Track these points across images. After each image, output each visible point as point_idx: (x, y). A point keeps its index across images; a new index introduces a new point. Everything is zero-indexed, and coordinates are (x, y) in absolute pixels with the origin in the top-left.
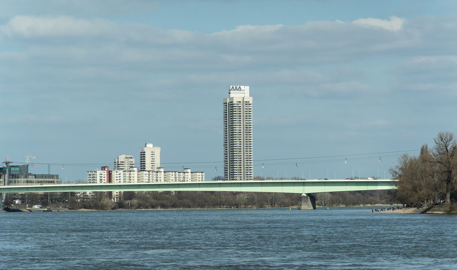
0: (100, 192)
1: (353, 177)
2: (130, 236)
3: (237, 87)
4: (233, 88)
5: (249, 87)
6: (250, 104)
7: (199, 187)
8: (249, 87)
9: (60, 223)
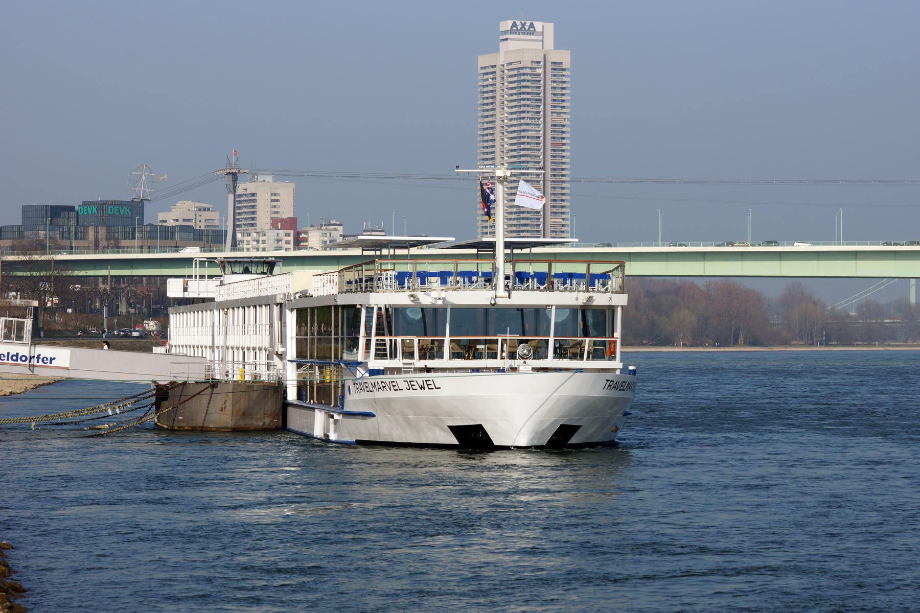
0: (702, 345)
1: (409, 265)
3: (525, 23)
4: (514, 25)
5: (552, 24)
6: (564, 70)
8: (552, 24)
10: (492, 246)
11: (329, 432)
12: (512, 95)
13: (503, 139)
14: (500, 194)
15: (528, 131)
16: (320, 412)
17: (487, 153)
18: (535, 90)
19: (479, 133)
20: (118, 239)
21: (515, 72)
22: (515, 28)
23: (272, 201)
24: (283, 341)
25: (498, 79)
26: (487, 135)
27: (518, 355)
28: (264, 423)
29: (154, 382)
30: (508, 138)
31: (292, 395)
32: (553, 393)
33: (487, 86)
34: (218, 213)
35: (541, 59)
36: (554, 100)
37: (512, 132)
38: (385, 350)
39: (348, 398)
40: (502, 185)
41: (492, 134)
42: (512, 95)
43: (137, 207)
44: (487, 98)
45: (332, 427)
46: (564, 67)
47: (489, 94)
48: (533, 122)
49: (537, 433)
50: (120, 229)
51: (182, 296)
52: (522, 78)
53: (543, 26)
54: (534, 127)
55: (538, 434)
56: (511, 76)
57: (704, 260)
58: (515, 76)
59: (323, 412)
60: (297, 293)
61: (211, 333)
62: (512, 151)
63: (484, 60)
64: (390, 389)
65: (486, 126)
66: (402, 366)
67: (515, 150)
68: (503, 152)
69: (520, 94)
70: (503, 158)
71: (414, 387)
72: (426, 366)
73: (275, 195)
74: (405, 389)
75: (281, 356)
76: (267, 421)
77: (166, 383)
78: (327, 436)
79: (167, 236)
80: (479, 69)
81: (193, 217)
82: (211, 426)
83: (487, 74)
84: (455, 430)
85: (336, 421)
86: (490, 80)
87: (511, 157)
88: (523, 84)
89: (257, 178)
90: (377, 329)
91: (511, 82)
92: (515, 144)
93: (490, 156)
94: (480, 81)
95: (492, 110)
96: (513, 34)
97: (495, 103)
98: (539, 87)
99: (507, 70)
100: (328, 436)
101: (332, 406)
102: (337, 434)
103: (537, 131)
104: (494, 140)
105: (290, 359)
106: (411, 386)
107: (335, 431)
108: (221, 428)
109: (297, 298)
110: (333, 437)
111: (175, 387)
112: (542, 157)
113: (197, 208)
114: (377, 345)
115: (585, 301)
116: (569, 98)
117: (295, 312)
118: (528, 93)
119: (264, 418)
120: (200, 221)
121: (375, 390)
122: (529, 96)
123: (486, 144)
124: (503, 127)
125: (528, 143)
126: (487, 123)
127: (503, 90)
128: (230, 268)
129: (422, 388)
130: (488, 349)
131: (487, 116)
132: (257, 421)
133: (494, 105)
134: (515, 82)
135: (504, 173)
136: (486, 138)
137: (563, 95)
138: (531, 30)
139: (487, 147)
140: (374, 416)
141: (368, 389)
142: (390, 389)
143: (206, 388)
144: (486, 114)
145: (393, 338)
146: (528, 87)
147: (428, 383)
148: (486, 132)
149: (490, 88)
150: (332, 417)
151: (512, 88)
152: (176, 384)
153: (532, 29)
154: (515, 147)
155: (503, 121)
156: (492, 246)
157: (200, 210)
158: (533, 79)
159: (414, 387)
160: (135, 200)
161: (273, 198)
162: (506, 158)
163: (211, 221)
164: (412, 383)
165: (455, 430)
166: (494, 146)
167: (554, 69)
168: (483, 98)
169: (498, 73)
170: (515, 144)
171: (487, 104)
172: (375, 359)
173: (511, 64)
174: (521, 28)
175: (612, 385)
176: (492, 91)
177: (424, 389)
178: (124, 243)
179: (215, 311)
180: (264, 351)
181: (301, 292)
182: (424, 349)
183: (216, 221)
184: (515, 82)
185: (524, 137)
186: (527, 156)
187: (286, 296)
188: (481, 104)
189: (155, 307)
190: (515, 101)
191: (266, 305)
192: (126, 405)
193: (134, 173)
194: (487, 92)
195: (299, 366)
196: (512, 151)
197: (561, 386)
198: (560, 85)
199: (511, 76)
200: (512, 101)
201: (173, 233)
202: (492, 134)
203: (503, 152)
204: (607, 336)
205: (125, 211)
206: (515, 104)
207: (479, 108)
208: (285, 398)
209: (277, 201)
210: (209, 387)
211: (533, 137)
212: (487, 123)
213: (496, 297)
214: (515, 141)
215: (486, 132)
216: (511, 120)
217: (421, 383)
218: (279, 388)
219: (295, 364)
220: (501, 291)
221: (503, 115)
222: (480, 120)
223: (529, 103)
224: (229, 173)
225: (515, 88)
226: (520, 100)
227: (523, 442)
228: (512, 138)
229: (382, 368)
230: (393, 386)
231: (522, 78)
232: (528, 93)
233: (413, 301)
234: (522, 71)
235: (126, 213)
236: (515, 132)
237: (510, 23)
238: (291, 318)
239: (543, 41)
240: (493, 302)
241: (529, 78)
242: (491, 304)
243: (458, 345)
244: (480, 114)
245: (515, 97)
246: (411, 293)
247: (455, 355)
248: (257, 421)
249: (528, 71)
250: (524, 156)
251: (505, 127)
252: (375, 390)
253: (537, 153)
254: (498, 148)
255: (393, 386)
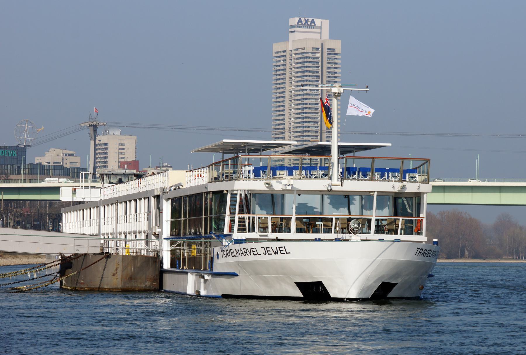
2: (302, 339)
3: (308, 20)
4: (300, 21)
5: (328, 21)
6: (336, 54)
7: (41, 194)
8: (328, 21)
9: (13, 304)
10: (326, 150)
11: (200, 289)
12: (297, 72)
13: (291, 105)
14: (335, 105)
15: (309, 99)
16: (192, 274)
17: (279, 115)
18: (315, 69)
19: (273, 100)
20: (7, 174)
21: (300, 56)
22: (300, 23)
23: (119, 149)
24: (160, 224)
25: (288, 61)
26: (279, 102)
27: (350, 228)
28: (146, 285)
29: (61, 254)
30: (294, 104)
31: (167, 265)
32: (377, 258)
33: (279, 66)
34: (79, 157)
35: (320, 46)
36: (329, 77)
37: (297, 100)
38: (245, 226)
39: (216, 262)
40: (337, 99)
41: (283, 101)
42: (297, 72)
43: (21, 151)
44: (279, 75)
45: (202, 285)
46: (336, 53)
47: (281, 72)
48: (313, 93)
49: (363, 290)
50: (9, 166)
51: (71, 200)
52: (306, 60)
53: (321, 22)
54: (314, 97)
55: (363, 291)
56: (297, 59)
57: (444, 192)
58: (300, 58)
59: (194, 275)
60: (172, 186)
61: (98, 224)
62: (297, 114)
63: (277, 47)
64: (251, 254)
65: (278, 95)
66: (258, 237)
67: (300, 113)
68: (291, 114)
69: (304, 72)
70: (291, 119)
71: (269, 252)
72: (277, 237)
73: (122, 145)
74: (262, 254)
75: (157, 236)
76: (148, 284)
77: (69, 255)
78: (198, 292)
79: (43, 173)
80: (274, 53)
81: (61, 161)
82: (106, 287)
83: (279, 57)
84: (300, 285)
85: (206, 281)
86: (282, 61)
87: (297, 118)
88: (306, 64)
89: (109, 132)
90: (239, 210)
91: (297, 63)
92: (299, 109)
93: (281, 117)
94: (274, 62)
95: (283, 83)
96: (299, 27)
97: (285, 78)
98: (318, 67)
99: (294, 54)
100: (199, 292)
101: (202, 269)
102: (206, 291)
103: (316, 99)
104: (284, 106)
105: (166, 237)
106: (267, 251)
107: (205, 289)
108: (113, 289)
109: (172, 190)
110: (203, 293)
111: (78, 257)
112: (319, 119)
113: (64, 154)
114: (239, 222)
115: (399, 189)
116: (340, 75)
117: (170, 201)
118: (310, 71)
119: (146, 282)
120: (66, 164)
121: (238, 255)
122: (310, 74)
123: (278, 109)
124: (291, 96)
125: (309, 108)
126: (279, 93)
127: (291, 69)
128: (108, 179)
129: (276, 253)
130: (324, 225)
131: (279, 88)
132: (141, 283)
133: (284, 80)
134: (300, 63)
135: (338, 90)
136: (278, 104)
137: (336, 73)
138: (312, 25)
139: (279, 111)
140: (237, 275)
141: (233, 255)
142: (251, 254)
143: (102, 258)
144: (278, 86)
145: (251, 216)
146: (309, 67)
147: (281, 249)
148: (278, 100)
149: (282, 67)
150: (203, 277)
151: (298, 68)
152: (79, 255)
153: (313, 24)
154: (299, 111)
155: (291, 92)
156: (326, 150)
157: (66, 155)
158: (314, 61)
159: (269, 252)
160: (20, 146)
161: (121, 147)
162: (293, 119)
163: (74, 164)
164: (268, 249)
165: (300, 285)
166: (284, 110)
167: (329, 54)
168: (277, 75)
169: (288, 57)
170: (299, 109)
171: (279, 79)
172: (238, 232)
173: (297, 49)
174: (305, 23)
175: (421, 252)
176: (283, 70)
177: (277, 254)
178: (12, 177)
179: (101, 207)
180: (143, 233)
181: (176, 185)
182: (275, 225)
183: (78, 164)
184: (300, 63)
185: (306, 104)
186: (309, 117)
187: (163, 190)
188: (275, 79)
189: (35, 223)
190: (300, 77)
191: (145, 198)
192: (41, 270)
193: (19, 126)
194: (279, 70)
195: (172, 244)
196: (297, 114)
197: (383, 252)
198: (334, 66)
199: (297, 59)
200: (298, 77)
201: (48, 170)
202: (283, 101)
203: (291, 114)
204: (414, 216)
205: (12, 153)
206: (300, 79)
207: (273, 82)
208: (162, 267)
209: (123, 149)
210: (104, 257)
211: (313, 104)
212: (279, 93)
213: (331, 185)
214: (299, 107)
215: (278, 100)
216: (297, 91)
217: (275, 249)
218: (157, 260)
219: (169, 241)
220: (335, 181)
221: (291, 88)
222: (274, 91)
223: (310, 78)
224: (91, 125)
225: (300, 67)
226: (304, 76)
227: (353, 295)
228: (297, 104)
229: (244, 238)
230: (253, 252)
231: (306, 60)
232: (310, 71)
233: (268, 187)
234: (305, 55)
235: (13, 155)
236: (300, 100)
237: (297, 19)
238: (167, 207)
239: (321, 33)
240: (329, 189)
241: (310, 60)
242: (328, 190)
243: (301, 222)
244: (274, 87)
245: (300, 74)
246: (266, 181)
247: (299, 230)
248: (141, 283)
249: (310, 55)
250: (306, 117)
251: (293, 96)
252: (238, 255)
253: (316, 116)
254: (287, 112)
255: (253, 251)
